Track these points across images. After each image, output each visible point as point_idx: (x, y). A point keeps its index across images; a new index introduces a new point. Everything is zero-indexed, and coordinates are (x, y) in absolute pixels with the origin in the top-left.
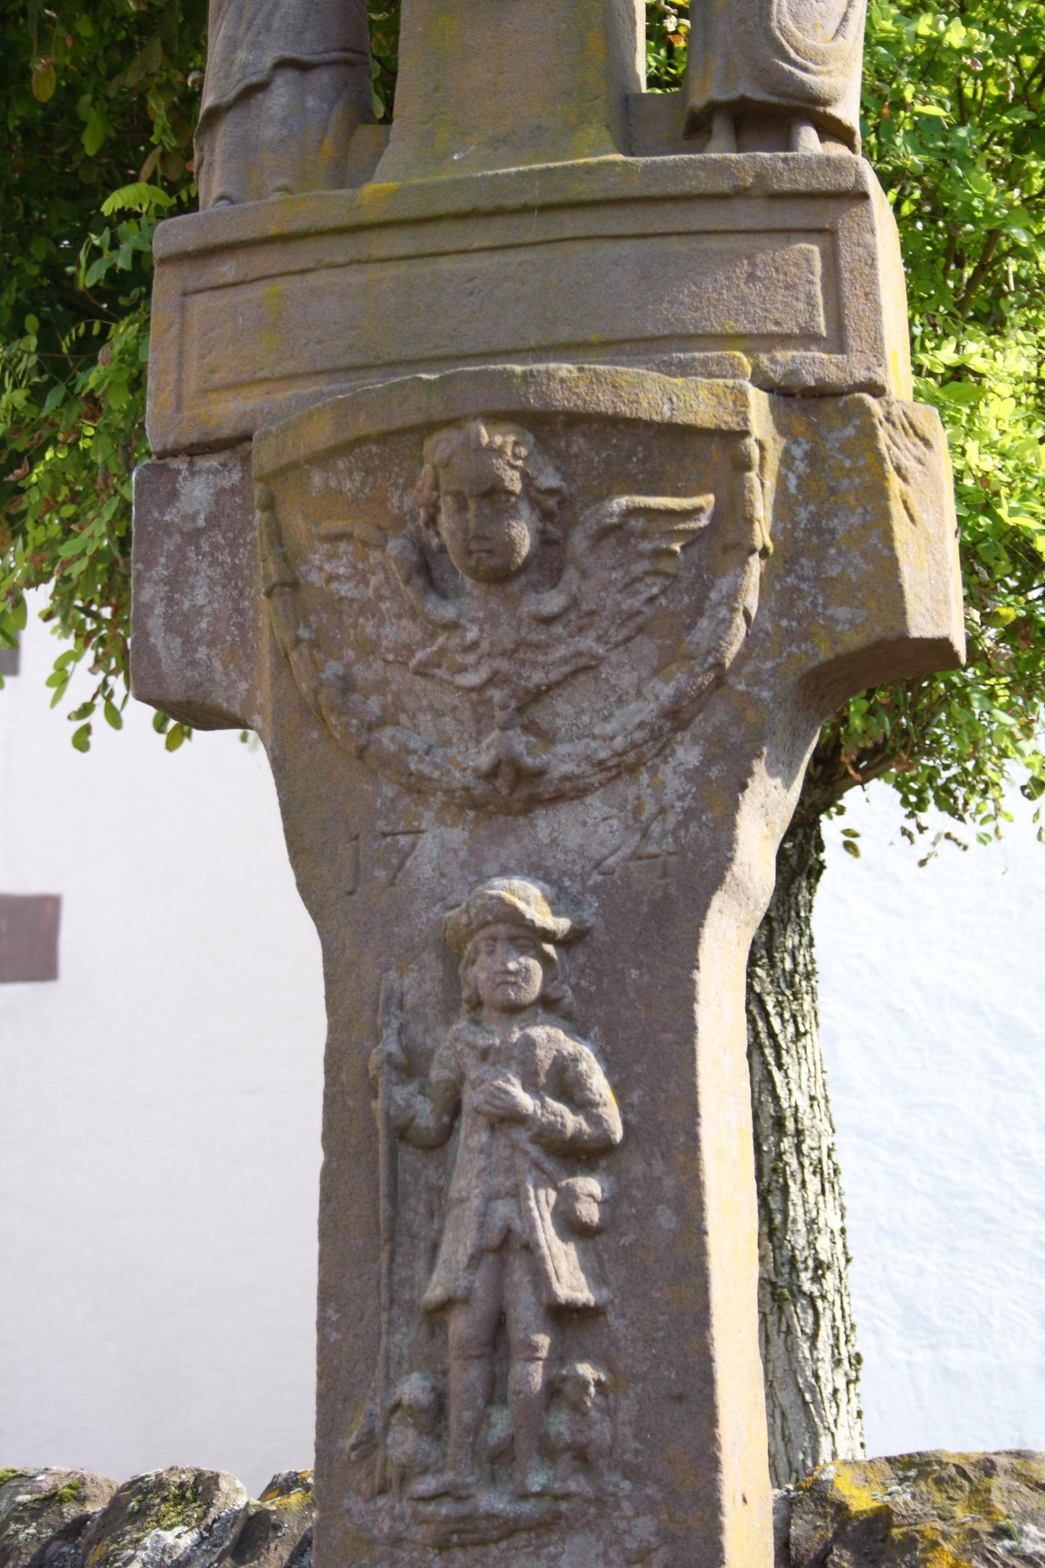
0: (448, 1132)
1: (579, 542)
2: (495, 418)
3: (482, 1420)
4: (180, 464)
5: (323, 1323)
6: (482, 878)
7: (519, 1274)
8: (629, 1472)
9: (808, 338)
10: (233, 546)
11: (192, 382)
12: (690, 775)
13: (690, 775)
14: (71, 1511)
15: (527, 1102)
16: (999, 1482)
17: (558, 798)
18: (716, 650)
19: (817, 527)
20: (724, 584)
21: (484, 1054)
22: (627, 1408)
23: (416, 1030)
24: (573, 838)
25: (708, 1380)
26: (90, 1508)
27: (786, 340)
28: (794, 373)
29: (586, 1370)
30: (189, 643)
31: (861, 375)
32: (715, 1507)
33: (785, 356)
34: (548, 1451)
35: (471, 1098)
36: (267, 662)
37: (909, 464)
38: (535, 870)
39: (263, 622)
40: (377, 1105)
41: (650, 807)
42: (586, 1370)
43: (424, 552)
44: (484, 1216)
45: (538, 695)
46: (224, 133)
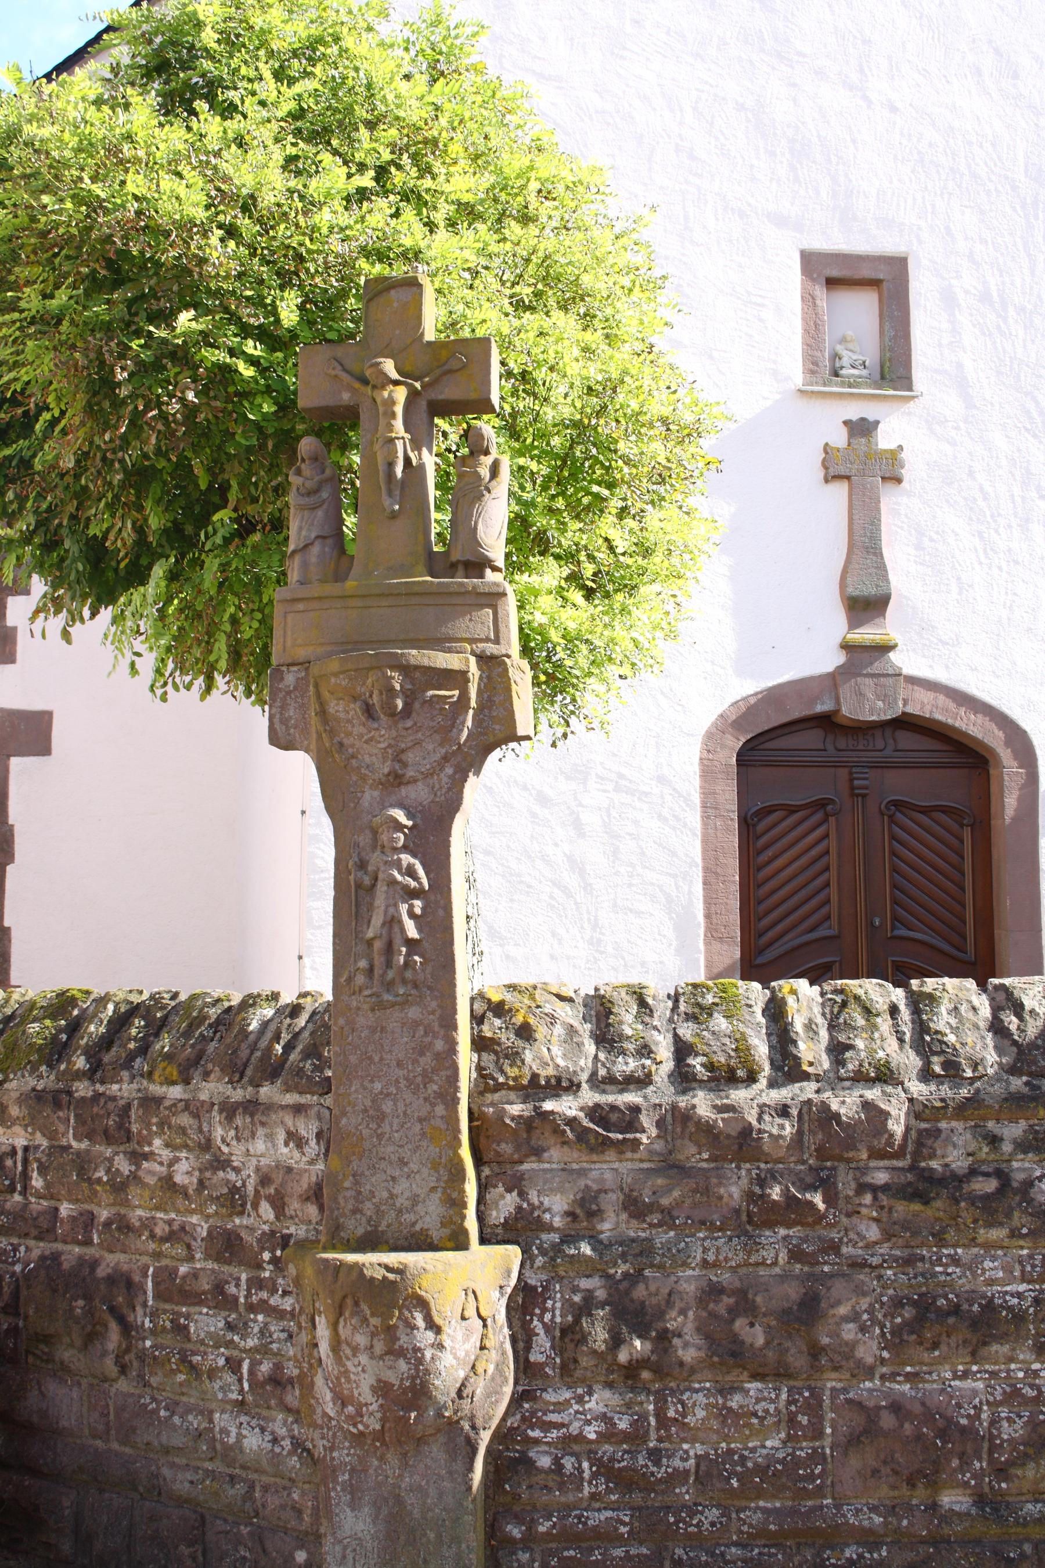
0: (374, 886)
1: (417, 705)
2: (392, 668)
3: (385, 973)
4: (284, 668)
5: (334, 944)
6: (384, 808)
7: (396, 929)
8: (429, 988)
9: (487, 640)
10: (302, 697)
11: (289, 643)
12: (449, 777)
13: (449, 777)
14: (226, 1004)
15: (399, 878)
16: (538, 992)
17: (408, 783)
18: (459, 739)
19: (490, 699)
20: (461, 718)
21: (386, 862)
22: (429, 969)
23: (363, 854)
24: (413, 795)
25: (453, 961)
26: (232, 1003)
27: (481, 640)
28: (483, 651)
29: (417, 958)
30: (288, 728)
31: (504, 652)
32: (455, 998)
33: (481, 645)
34: (404, 982)
35: (381, 876)
36: (314, 736)
37: (518, 680)
38: (401, 806)
39: (313, 722)
40: (352, 877)
41: (437, 786)
42: (417, 958)
43: (367, 705)
44: (386, 912)
45: (403, 751)
46: (297, 560)
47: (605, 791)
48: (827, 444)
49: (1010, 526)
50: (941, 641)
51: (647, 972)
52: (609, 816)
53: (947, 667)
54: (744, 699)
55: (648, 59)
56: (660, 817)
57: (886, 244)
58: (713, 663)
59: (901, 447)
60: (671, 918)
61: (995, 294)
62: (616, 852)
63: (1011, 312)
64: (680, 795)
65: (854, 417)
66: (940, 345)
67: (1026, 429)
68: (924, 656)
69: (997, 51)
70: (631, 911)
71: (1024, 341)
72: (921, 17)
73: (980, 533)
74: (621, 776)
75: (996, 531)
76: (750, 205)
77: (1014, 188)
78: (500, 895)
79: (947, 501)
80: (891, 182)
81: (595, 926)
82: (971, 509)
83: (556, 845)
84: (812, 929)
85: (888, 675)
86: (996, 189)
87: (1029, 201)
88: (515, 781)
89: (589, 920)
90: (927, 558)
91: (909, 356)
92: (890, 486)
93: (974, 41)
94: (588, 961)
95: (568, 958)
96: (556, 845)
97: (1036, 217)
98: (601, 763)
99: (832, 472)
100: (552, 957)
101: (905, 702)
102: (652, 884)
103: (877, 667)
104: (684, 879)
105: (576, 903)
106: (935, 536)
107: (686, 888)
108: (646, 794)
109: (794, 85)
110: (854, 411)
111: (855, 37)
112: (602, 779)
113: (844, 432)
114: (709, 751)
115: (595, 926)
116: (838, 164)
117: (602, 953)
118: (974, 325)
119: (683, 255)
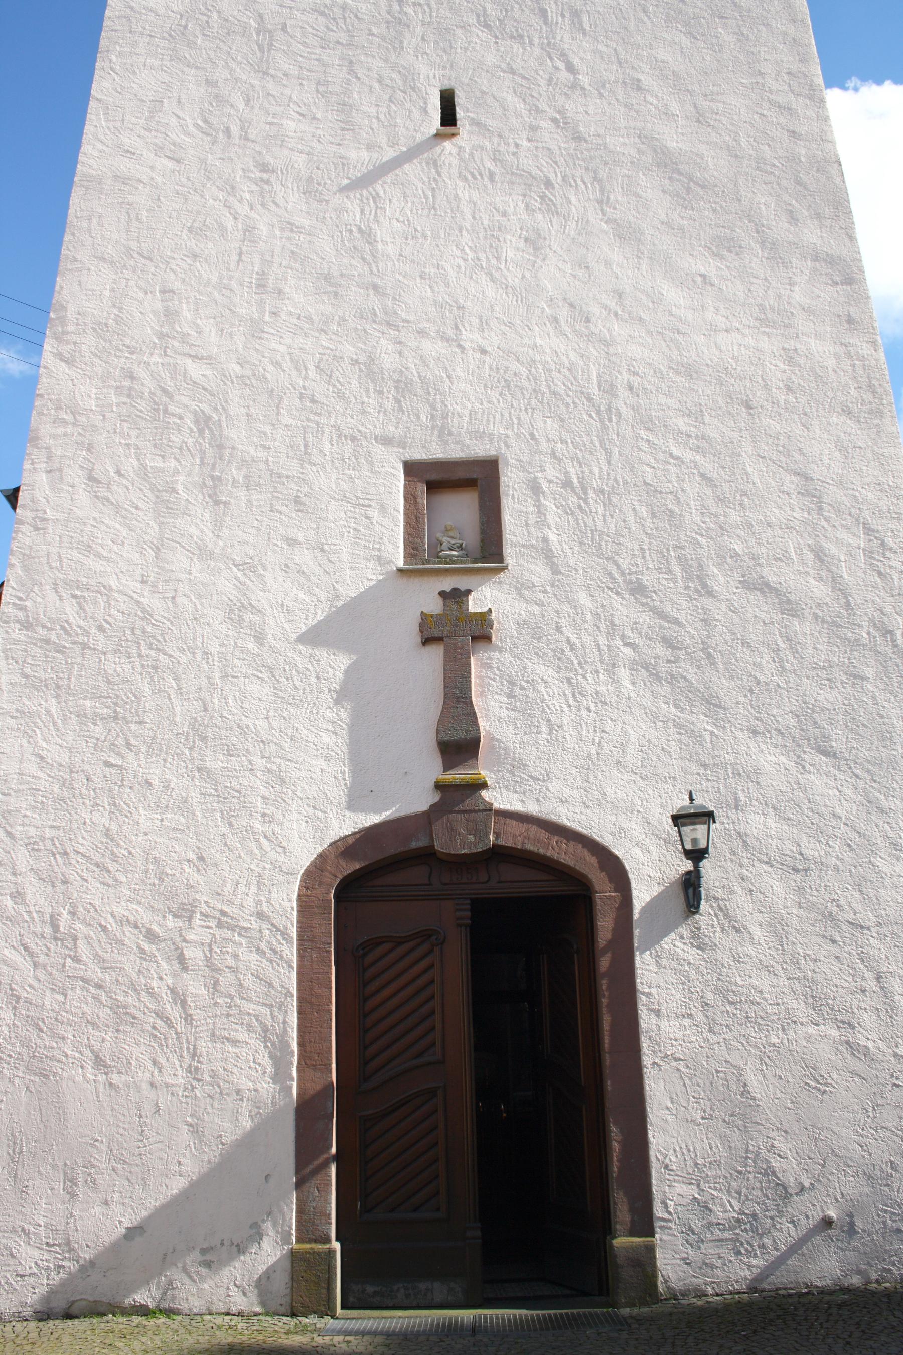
47: (208, 927)
48: (422, 612)
49: (597, 672)
50: (531, 777)
51: (241, 1100)
52: (211, 950)
53: (538, 801)
54: (341, 839)
55: (281, 337)
56: (258, 950)
57: (480, 450)
58: (314, 808)
59: (490, 610)
60: (266, 1047)
61: (575, 481)
62: (216, 983)
63: (591, 494)
64: (278, 930)
65: (448, 588)
66: (527, 525)
67: (609, 588)
68: (516, 792)
69: (572, 305)
70: (228, 1039)
71: (604, 516)
72: (506, 288)
73: (569, 681)
74: (224, 913)
75: (584, 677)
76: (360, 431)
77: (590, 400)
78: (107, 1026)
79: (537, 654)
80: (482, 404)
81: (194, 1055)
82: (559, 659)
83: (161, 978)
84: (420, 1055)
85: (479, 811)
86: (574, 402)
87: (602, 408)
88: (128, 921)
89: (188, 1048)
90: (518, 704)
91: (501, 536)
92: (481, 645)
93: (551, 300)
94: (185, 1089)
95: (167, 1086)
96: (161, 978)
97: (610, 420)
98: (206, 902)
99: (426, 635)
100: (152, 1085)
101: (498, 835)
102: (249, 1014)
103: (468, 804)
104: (280, 1009)
105: (176, 1033)
106: (525, 685)
107: (281, 1018)
108: (246, 929)
109: (400, 343)
110: (447, 584)
111: (451, 306)
112: (206, 916)
113: (440, 601)
114: (307, 888)
115: (194, 1055)
116: (436, 395)
117: (199, 1080)
118: (558, 508)
119: (302, 473)
